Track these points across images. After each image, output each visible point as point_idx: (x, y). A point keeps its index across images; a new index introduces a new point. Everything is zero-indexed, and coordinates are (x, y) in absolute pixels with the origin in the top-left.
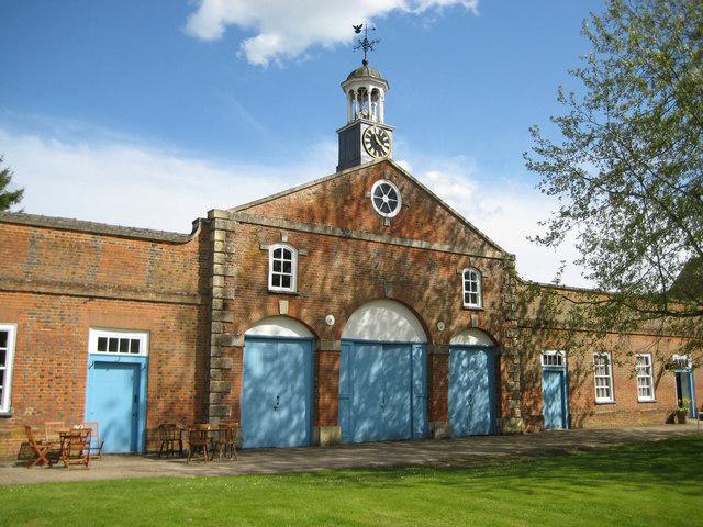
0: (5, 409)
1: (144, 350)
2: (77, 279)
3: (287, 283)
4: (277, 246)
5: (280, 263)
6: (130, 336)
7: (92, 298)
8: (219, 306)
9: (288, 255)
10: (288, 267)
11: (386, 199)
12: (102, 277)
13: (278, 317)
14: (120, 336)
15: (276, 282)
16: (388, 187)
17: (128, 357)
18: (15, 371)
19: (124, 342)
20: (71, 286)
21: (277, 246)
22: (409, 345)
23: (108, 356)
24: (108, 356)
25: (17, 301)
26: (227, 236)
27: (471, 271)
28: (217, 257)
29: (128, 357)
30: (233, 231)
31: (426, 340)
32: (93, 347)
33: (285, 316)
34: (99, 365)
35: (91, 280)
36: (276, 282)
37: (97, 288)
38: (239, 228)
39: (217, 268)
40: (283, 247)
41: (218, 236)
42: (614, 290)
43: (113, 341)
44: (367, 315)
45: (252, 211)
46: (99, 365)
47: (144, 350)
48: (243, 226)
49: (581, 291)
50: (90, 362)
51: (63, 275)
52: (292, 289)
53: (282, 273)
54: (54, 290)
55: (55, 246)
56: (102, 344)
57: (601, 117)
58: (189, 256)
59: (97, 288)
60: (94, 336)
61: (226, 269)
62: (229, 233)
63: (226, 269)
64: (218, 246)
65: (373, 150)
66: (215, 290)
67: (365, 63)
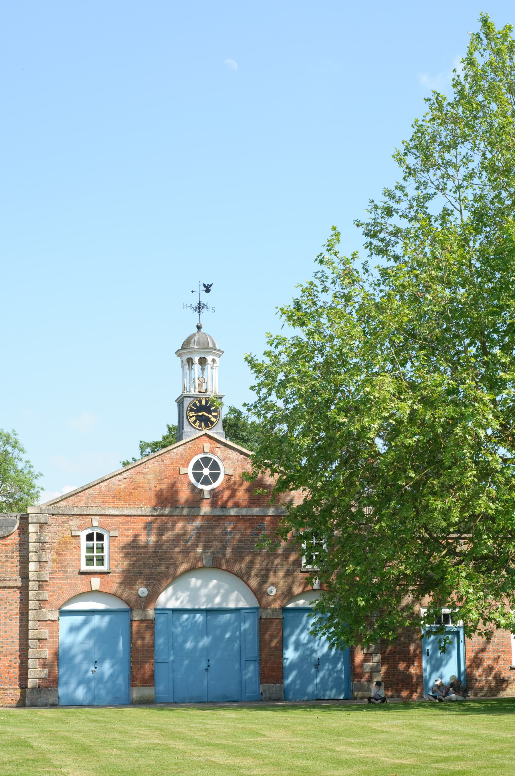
3: (101, 561)
5: (97, 540)
8: (36, 587)
15: (89, 561)
18: (109, 556)
21: (89, 531)
26: (41, 528)
28: (32, 547)
30: (46, 523)
31: (255, 604)
33: (97, 591)
38: (50, 520)
41: (32, 528)
44: (215, 582)
45: (63, 504)
48: (55, 517)
53: (95, 554)
58: (10, 547)
61: (40, 556)
62: (42, 525)
63: (40, 556)
64: (32, 537)
65: (198, 423)
66: (30, 574)
67: (199, 327)
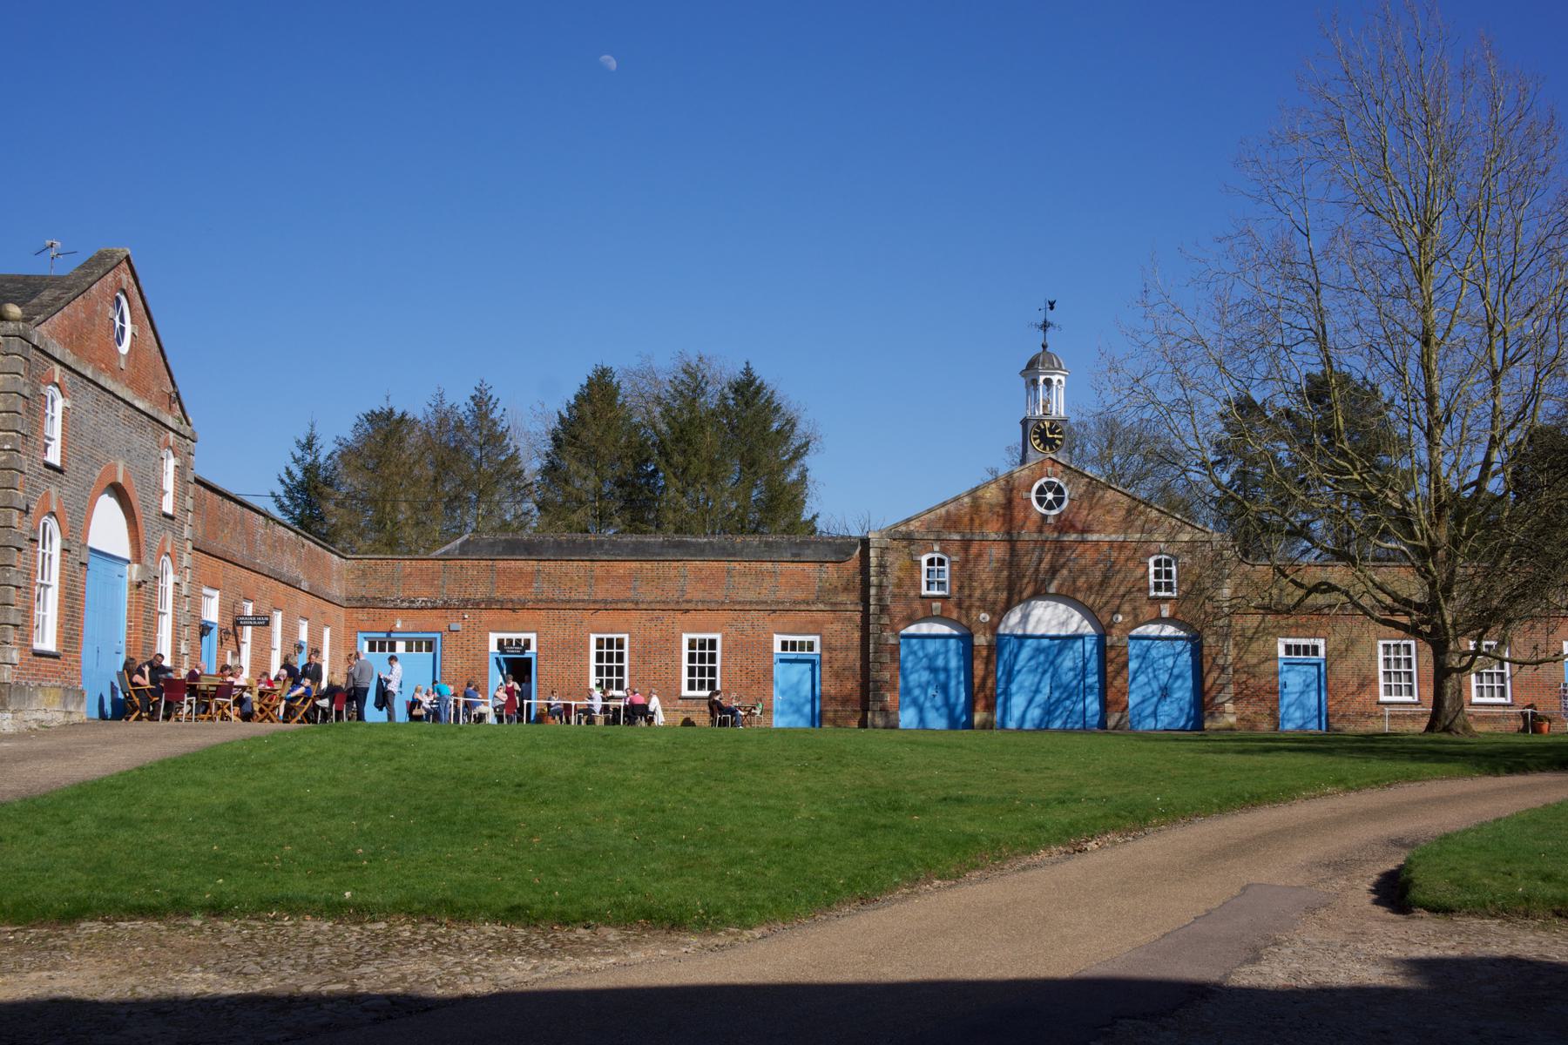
2: (762, 597)
6: (807, 638)
7: (687, 611)
12: (781, 595)
13: (1159, 620)
14: (797, 638)
17: (1314, 659)
20: (757, 603)
22: (1082, 637)
23: (790, 654)
24: (790, 654)
25: (723, 617)
27: (1164, 557)
28: (873, 570)
29: (1314, 659)
32: (777, 648)
34: (782, 661)
35: (773, 597)
37: (616, 602)
39: (874, 580)
40: (936, 556)
43: (794, 643)
46: (782, 661)
47: (1322, 651)
50: (775, 658)
54: (744, 607)
55: (745, 574)
56: (784, 645)
60: (778, 640)
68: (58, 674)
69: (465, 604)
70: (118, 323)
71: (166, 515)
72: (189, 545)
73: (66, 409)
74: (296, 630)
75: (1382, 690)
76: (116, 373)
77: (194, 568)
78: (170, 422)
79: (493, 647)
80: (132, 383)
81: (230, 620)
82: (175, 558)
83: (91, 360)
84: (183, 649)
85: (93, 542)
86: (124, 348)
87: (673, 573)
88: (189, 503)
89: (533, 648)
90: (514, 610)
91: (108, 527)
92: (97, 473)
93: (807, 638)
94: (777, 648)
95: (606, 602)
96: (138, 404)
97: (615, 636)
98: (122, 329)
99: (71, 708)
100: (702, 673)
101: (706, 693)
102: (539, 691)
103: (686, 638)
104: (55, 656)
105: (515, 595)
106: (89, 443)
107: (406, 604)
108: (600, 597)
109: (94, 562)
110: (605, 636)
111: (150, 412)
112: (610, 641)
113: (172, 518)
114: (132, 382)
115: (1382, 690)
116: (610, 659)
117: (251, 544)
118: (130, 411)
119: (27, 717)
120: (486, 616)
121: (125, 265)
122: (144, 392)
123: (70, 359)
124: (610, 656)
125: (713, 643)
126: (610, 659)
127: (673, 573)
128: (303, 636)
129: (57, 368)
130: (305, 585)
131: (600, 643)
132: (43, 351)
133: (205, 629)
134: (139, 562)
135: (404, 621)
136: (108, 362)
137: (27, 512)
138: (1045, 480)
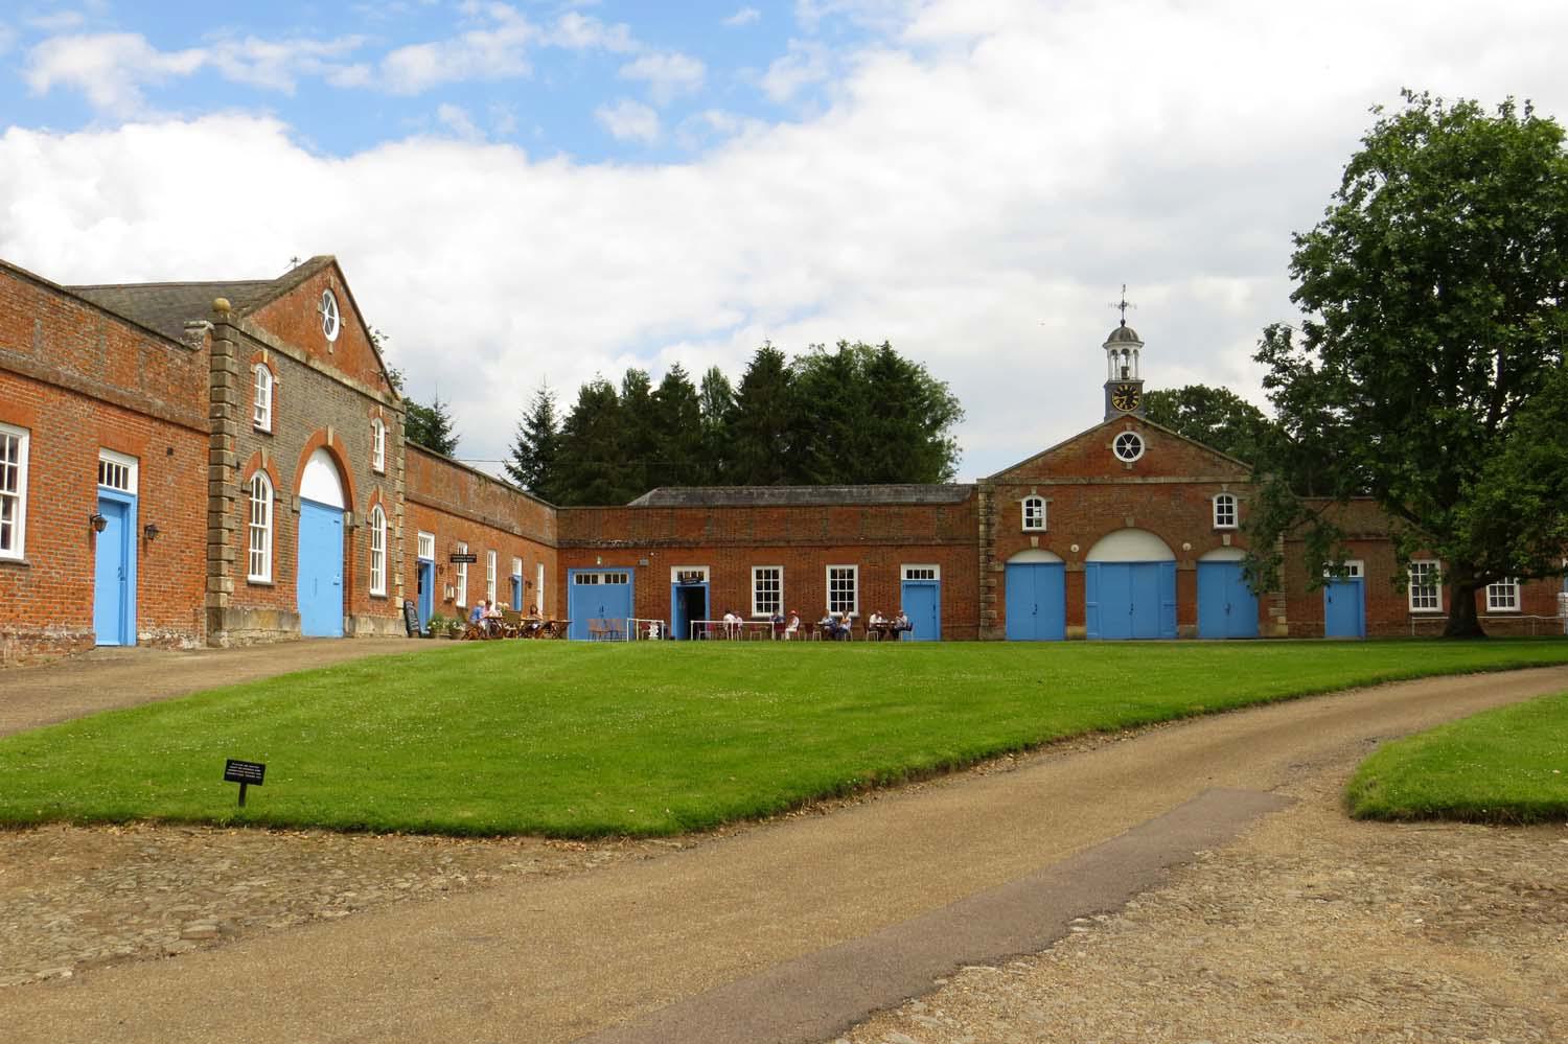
0: (16, 551)
1: (937, 577)
3: (1230, 521)
4: (1029, 498)
7: (901, 546)
9: (1229, 500)
10: (1230, 510)
11: (1128, 446)
15: (1221, 521)
16: (1139, 443)
19: (924, 572)
21: (1029, 498)
32: (904, 577)
34: (907, 586)
36: (1221, 521)
42: (1482, 217)
43: (917, 572)
47: (937, 577)
49: (139, 471)
51: (881, 534)
52: (1235, 525)
56: (909, 574)
57: (822, 364)
59: (904, 539)
68: (274, 600)
69: (650, 546)
70: (327, 316)
71: (376, 473)
72: (401, 497)
73: (275, 385)
74: (510, 567)
75: (1215, 520)
76: (326, 357)
77: (407, 517)
78: (379, 396)
79: (674, 579)
80: (342, 364)
81: (445, 558)
82: (388, 507)
83: (299, 345)
84: (398, 581)
85: (304, 492)
86: (332, 337)
87: (818, 516)
88: (400, 463)
89: (706, 579)
90: (690, 549)
91: (319, 482)
92: (308, 438)
93: (847, 567)
94: (904, 577)
95: (762, 541)
96: (345, 381)
97: (771, 568)
98: (332, 321)
99: (287, 628)
100: (768, 598)
101: (770, 614)
102: (711, 613)
103: (828, 569)
104: (269, 587)
105: (692, 537)
106: (299, 413)
107: (604, 546)
108: (759, 537)
109: (304, 510)
110: (763, 568)
111: (359, 389)
112: (768, 572)
113: (382, 475)
114: (339, 364)
115: (1215, 520)
116: (842, 587)
117: (465, 499)
118: (339, 388)
119: (243, 636)
120: (668, 554)
121: (331, 269)
122: (353, 372)
123: (278, 344)
124: (842, 584)
125: (851, 574)
126: (842, 587)
127: (818, 516)
128: (518, 572)
129: (266, 351)
130: (517, 530)
131: (759, 573)
132: (250, 337)
133: (422, 568)
134: (351, 510)
135: (603, 559)
136: (316, 344)
137: (238, 467)
138: (1115, 442)
